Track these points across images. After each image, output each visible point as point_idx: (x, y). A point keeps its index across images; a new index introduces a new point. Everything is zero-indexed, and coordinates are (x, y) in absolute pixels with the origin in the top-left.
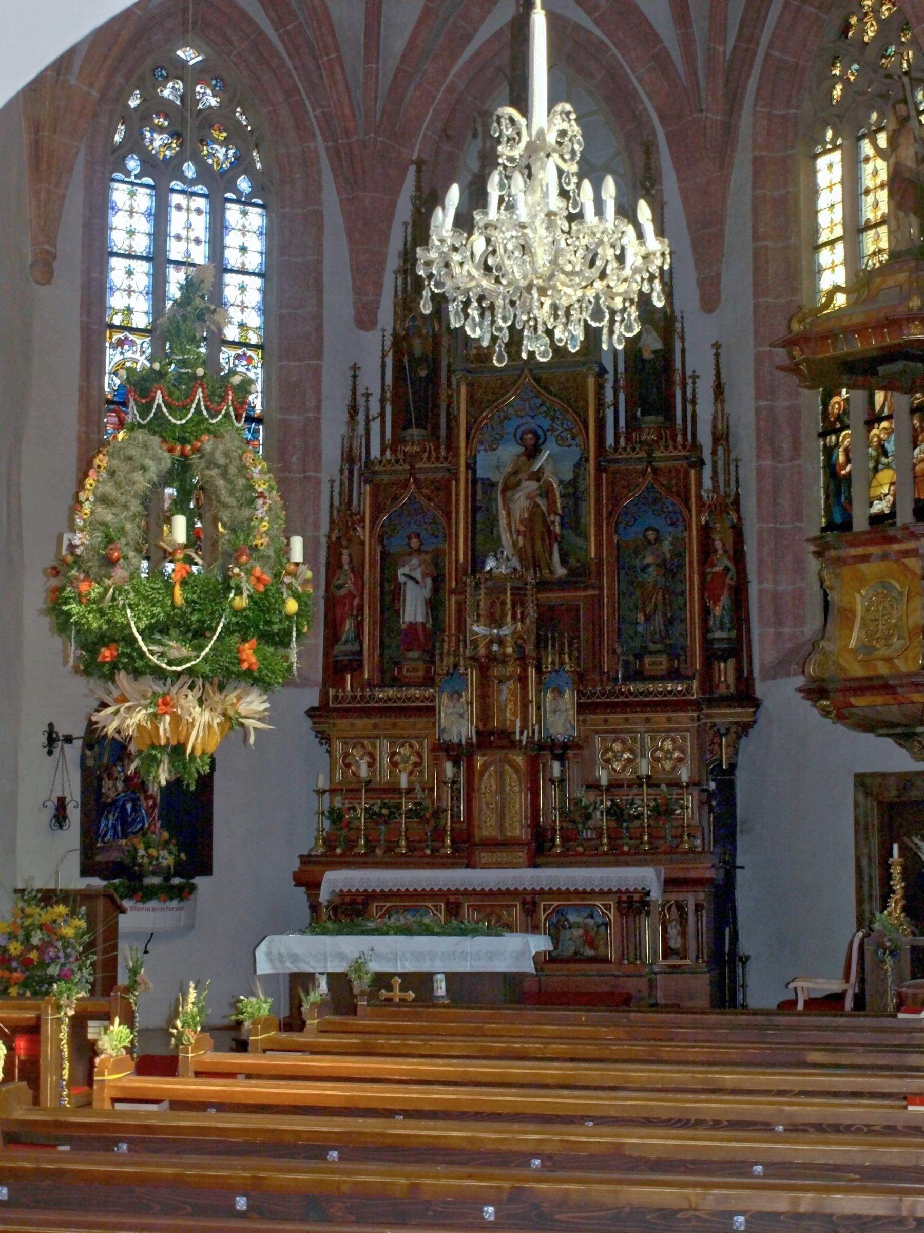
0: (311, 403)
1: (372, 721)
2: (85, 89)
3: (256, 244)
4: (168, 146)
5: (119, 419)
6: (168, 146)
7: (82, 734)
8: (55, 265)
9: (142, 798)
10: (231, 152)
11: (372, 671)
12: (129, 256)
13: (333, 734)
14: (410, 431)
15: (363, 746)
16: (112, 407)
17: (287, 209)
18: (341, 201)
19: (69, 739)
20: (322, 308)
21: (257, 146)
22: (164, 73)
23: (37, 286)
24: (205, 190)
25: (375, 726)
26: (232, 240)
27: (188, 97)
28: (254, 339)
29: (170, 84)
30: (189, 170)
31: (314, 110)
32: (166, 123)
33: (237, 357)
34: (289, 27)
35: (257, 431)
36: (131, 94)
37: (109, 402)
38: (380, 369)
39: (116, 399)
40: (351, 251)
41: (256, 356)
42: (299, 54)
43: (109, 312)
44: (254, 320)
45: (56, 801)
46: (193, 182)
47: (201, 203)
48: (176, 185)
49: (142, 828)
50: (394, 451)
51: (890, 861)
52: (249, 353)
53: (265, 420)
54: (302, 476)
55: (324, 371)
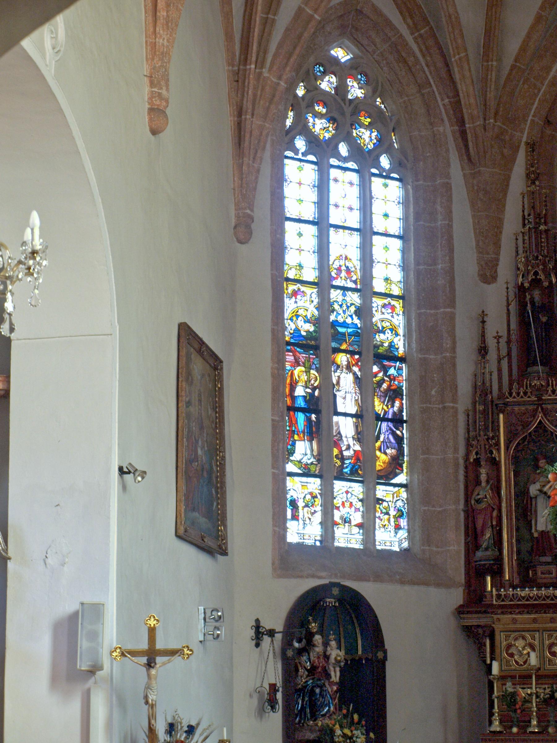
0: (447, 344)
1: (533, 616)
2: (275, 80)
3: (397, 212)
4: (325, 129)
5: (295, 359)
6: (325, 129)
7: (281, 630)
8: (253, 226)
9: (327, 684)
10: (374, 134)
11: (511, 573)
12: (299, 221)
13: (497, 627)
14: (535, 368)
15: (524, 638)
16: (289, 348)
17: (421, 182)
18: (464, 175)
19: (271, 633)
20: (453, 264)
21: (393, 131)
22: (321, 69)
23: (239, 245)
24: (355, 166)
25: (535, 621)
26: (377, 208)
27: (341, 89)
28: (396, 291)
29: (327, 78)
30: (343, 149)
31: (442, 100)
32: (324, 111)
33: (384, 306)
34: (422, 31)
35: (400, 369)
36: (297, 86)
37: (288, 343)
38: (505, 316)
39: (292, 341)
40: (473, 216)
41: (398, 305)
42: (430, 54)
43: (286, 267)
44: (397, 275)
45: (268, 688)
46: (345, 160)
47: (354, 177)
48: (333, 161)
49: (329, 710)
50: (520, 385)
51: (494, 711)
52: (393, 303)
53: (408, 359)
54: (441, 406)
55: (457, 317)
